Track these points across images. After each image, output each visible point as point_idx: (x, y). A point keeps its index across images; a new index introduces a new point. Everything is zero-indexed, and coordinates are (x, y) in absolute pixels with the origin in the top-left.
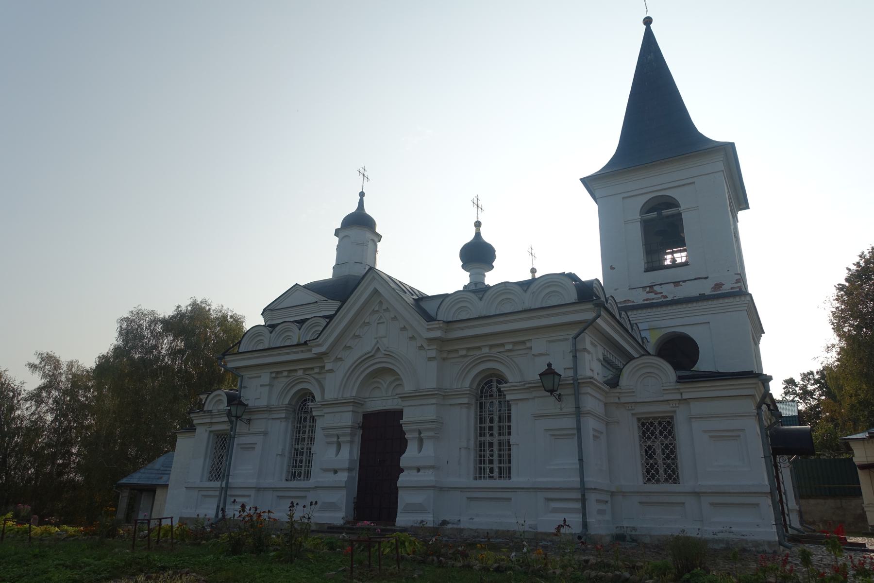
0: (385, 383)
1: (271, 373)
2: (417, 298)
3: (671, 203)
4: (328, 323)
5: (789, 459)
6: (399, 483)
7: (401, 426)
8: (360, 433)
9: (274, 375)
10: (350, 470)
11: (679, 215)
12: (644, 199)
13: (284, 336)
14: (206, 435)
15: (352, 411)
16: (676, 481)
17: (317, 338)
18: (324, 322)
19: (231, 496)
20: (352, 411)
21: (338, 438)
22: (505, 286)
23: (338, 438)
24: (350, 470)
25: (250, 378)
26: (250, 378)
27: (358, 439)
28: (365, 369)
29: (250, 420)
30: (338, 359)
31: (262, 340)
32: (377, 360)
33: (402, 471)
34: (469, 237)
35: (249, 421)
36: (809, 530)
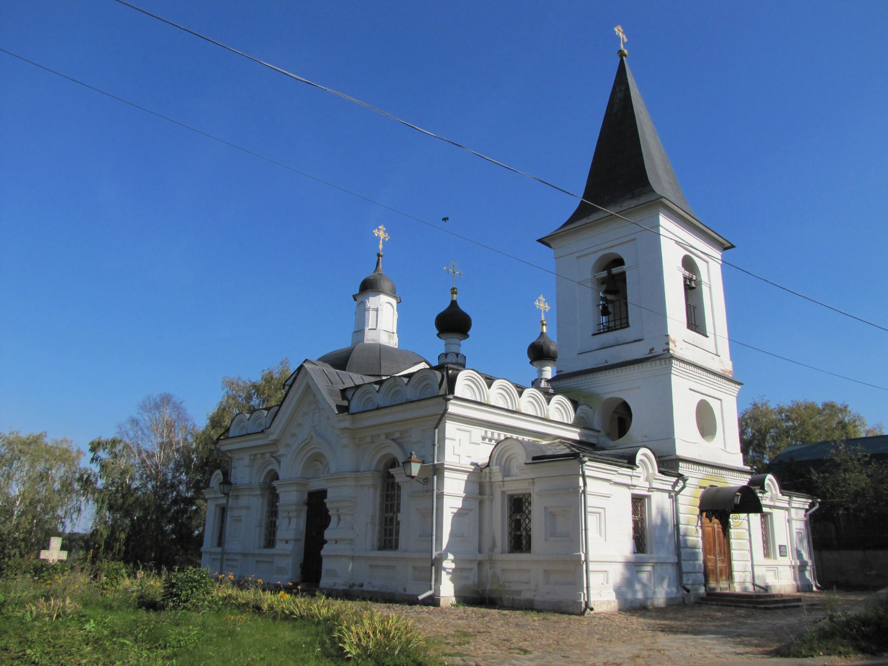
0: (322, 464)
1: (250, 455)
2: (428, 367)
3: (619, 262)
4: (408, 381)
5: (761, 497)
6: (323, 553)
7: (325, 504)
8: (306, 508)
9: (252, 457)
10: (297, 540)
11: (623, 274)
12: (594, 258)
13: (392, 392)
14: (213, 507)
15: (297, 491)
16: (528, 549)
17: (270, 427)
18: (277, 407)
19: (227, 560)
20: (297, 491)
21: (289, 513)
22: (558, 339)
23: (289, 513)
24: (297, 540)
25: (238, 459)
26: (238, 459)
27: (304, 515)
28: (308, 452)
29: (238, 496)
30: (288, 445)
31: (428, 384)
32: (313, 446)
33: (326, 542)
34: (444, 306)
35: (237, 497)
36: (586, 600)
